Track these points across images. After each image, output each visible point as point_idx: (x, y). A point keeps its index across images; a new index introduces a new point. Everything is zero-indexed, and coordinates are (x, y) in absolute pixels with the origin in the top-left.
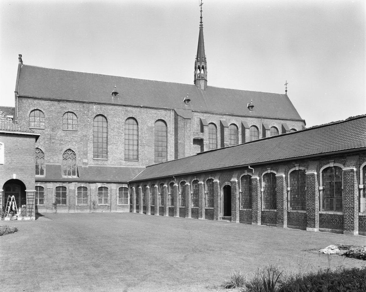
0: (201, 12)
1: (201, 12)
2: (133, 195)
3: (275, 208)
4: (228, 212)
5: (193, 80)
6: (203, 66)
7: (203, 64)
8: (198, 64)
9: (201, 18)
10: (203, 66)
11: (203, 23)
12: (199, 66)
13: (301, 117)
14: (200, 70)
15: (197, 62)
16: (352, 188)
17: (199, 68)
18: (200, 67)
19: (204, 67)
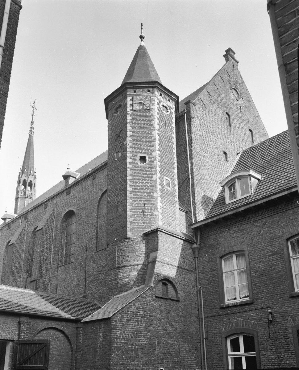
0: (33, 116)
1: (33, 116)
2: (147, 278)
3: (253, 350)
4: (288, 84)
5: (14, 197)
6: (31, 181)
7: (31, 178)
8: (24, 177)
9: (32, 122)
10: (31, 181)
11: (30, 126)
12: (25, 180)
13: (4, 122)
14: (25, 187)
15: (23, 174)
16: (146, 203)
17: (25, 184)
18: (26, 180)
19: (33, 182)
